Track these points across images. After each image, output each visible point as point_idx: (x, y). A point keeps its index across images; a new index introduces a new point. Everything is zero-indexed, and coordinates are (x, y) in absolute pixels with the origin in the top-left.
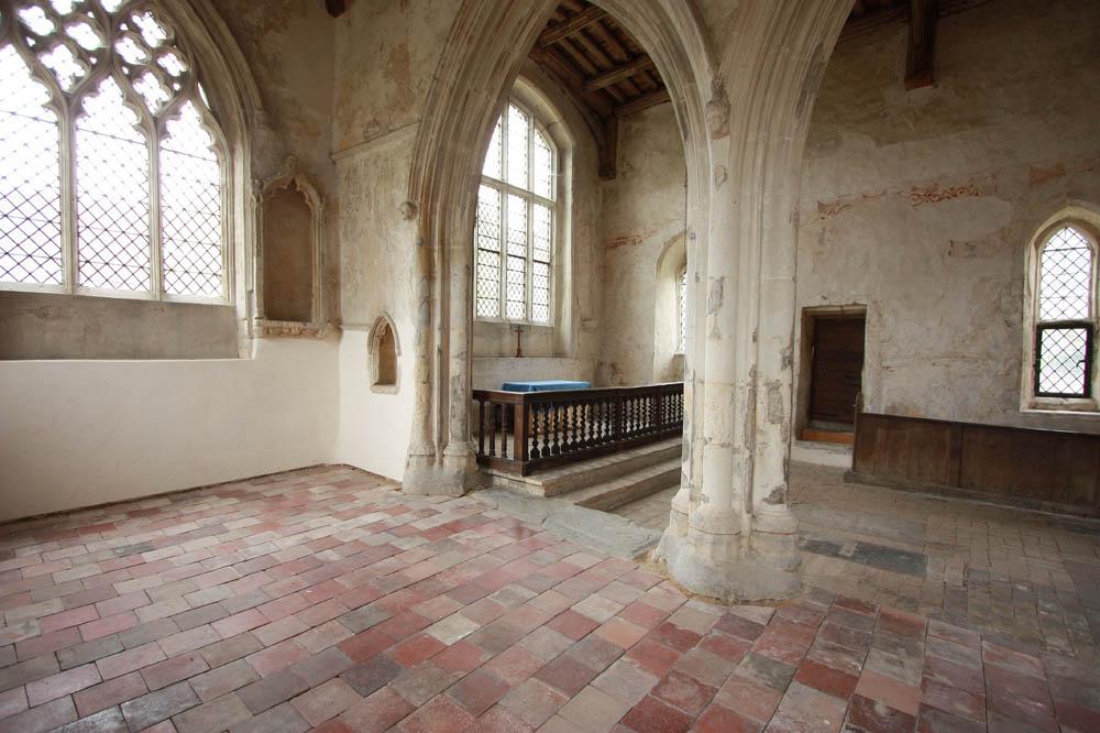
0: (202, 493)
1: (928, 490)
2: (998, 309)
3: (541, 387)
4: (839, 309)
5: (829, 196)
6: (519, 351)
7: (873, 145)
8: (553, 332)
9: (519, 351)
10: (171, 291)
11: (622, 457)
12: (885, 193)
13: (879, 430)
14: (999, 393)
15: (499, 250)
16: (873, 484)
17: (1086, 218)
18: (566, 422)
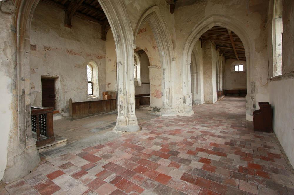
1: (87, 116)
2: (84, 79)
4: (51, 77)
5: (47, 45)
7: (58, 36)
12: (61, 49)
14: (85, 95)
16: (78, 119)
18: (219, 79)
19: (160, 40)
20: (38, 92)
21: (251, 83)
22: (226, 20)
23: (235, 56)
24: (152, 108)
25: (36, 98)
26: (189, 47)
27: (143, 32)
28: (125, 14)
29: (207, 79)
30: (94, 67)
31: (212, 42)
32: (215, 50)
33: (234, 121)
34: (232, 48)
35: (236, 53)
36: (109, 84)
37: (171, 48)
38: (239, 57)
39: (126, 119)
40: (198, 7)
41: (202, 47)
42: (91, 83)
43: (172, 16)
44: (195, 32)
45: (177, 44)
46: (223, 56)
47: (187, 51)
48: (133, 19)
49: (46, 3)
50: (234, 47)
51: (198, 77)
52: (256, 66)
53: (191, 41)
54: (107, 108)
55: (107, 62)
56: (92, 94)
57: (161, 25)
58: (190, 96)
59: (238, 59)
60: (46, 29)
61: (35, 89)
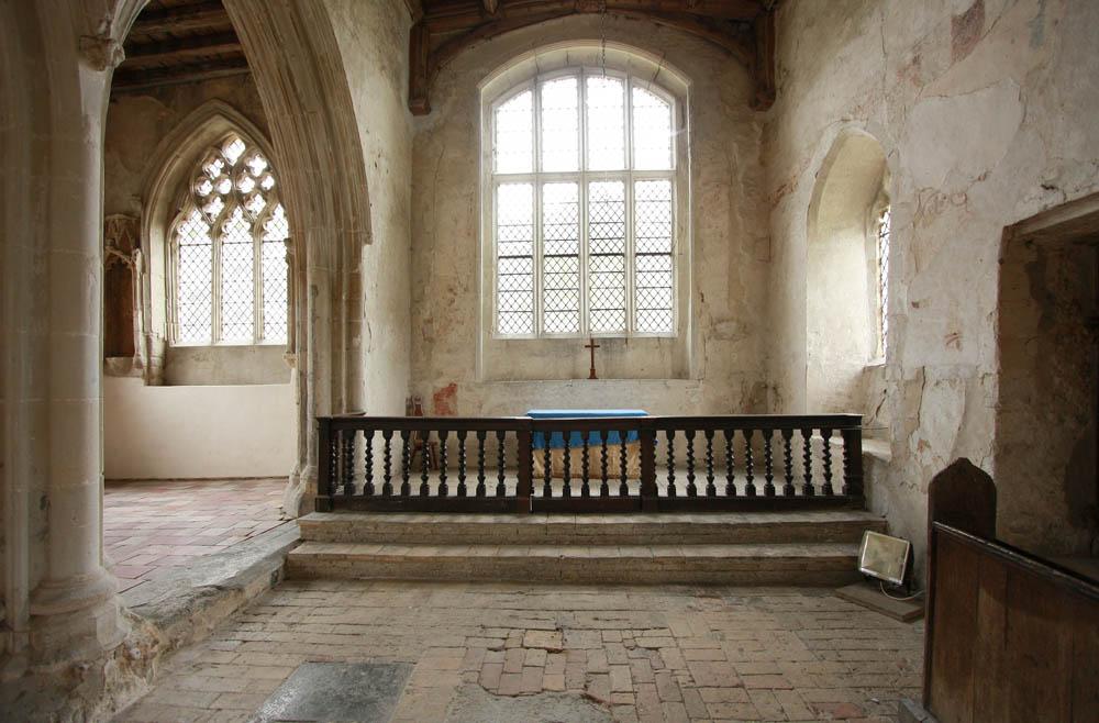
0: (208, 483)
3: (100, 421)
6: (593, 371)
8: (672, 344)
9: (593, 371)
10: (641, 330)
11: (997, 547)
13: (984, 595)
15: (623, 251)
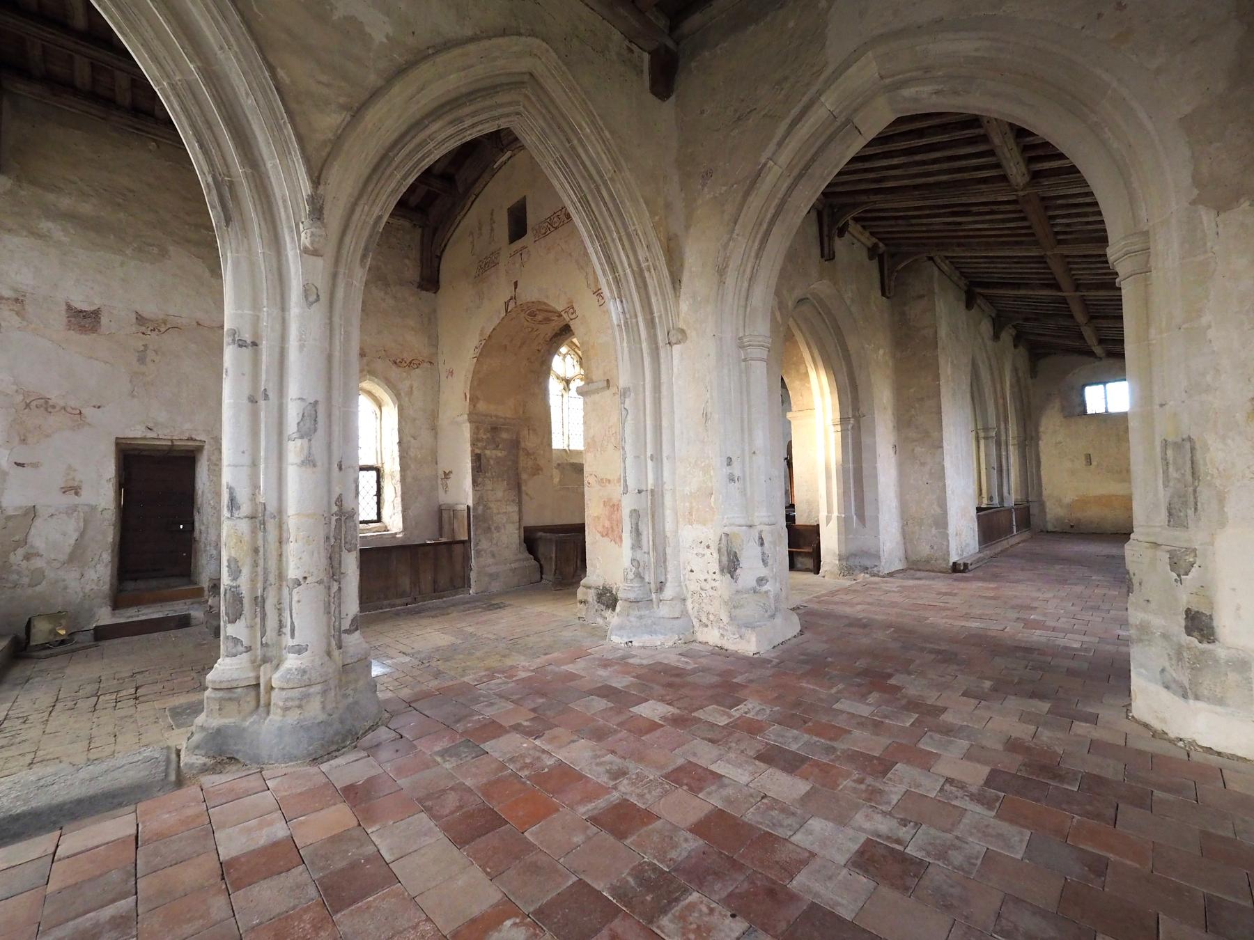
4: (170, 443)
5: (150, 309)
17: (373, 391)
19: (590, 236)
20: (93, 508)
21: (1165, 444)
22: (967, 45)
23: (1081, 337)
24: (593, 591)
25: (82, 535)
26: (752, 259)
27: (556, 228)
28: (237, 40)
29: (918, 450)
30: (388, 404)
31: (938, 261)
32: (962, 306)
33: (1025, 717)
34: (1056, 286)
35: (1080, 317)
36: (447, 475)
37: (657, 279)
38: (1101, 342)
39: (258, 678)
40: (791, 24)
41: (883, 294)
42: (374, 473)
43: (666, 111)
44: (776, 170)
45: (694, 258)
46: (1018, 340)
47: (746, 284)
48: (324, 78)
49: (154, 140)
50: (1064, 281)
51: (865, 440)
52: (1205, 320)
53: (765, 226)
54: (416, 582)
55: (443, 378)
56: (379, 520)
57: (586, 151)
58: (761, 538)
59: (1098, 350)
60: (153, 245)
61: (83, 493)
